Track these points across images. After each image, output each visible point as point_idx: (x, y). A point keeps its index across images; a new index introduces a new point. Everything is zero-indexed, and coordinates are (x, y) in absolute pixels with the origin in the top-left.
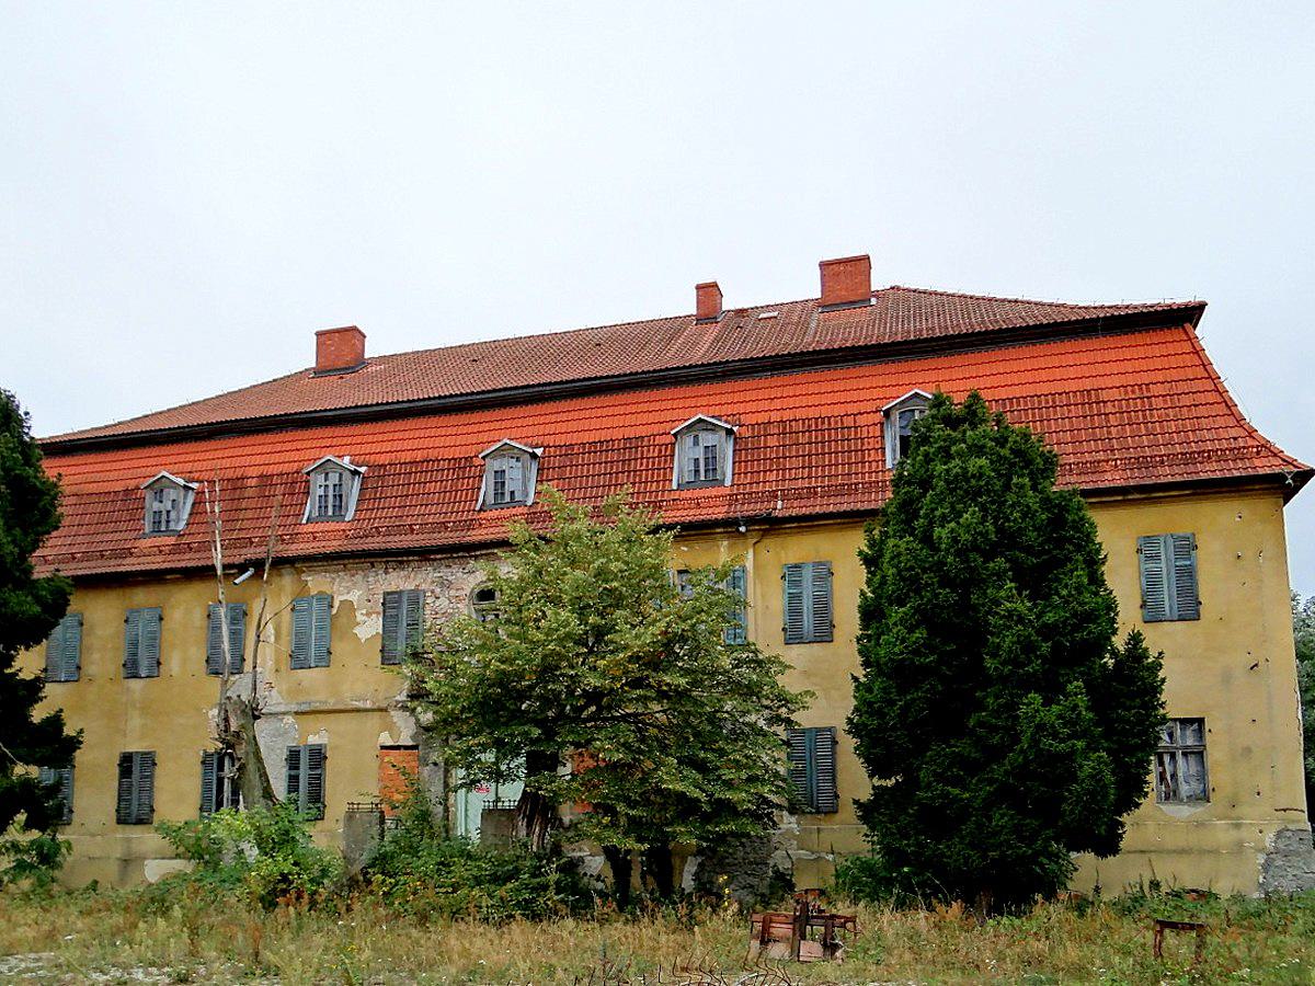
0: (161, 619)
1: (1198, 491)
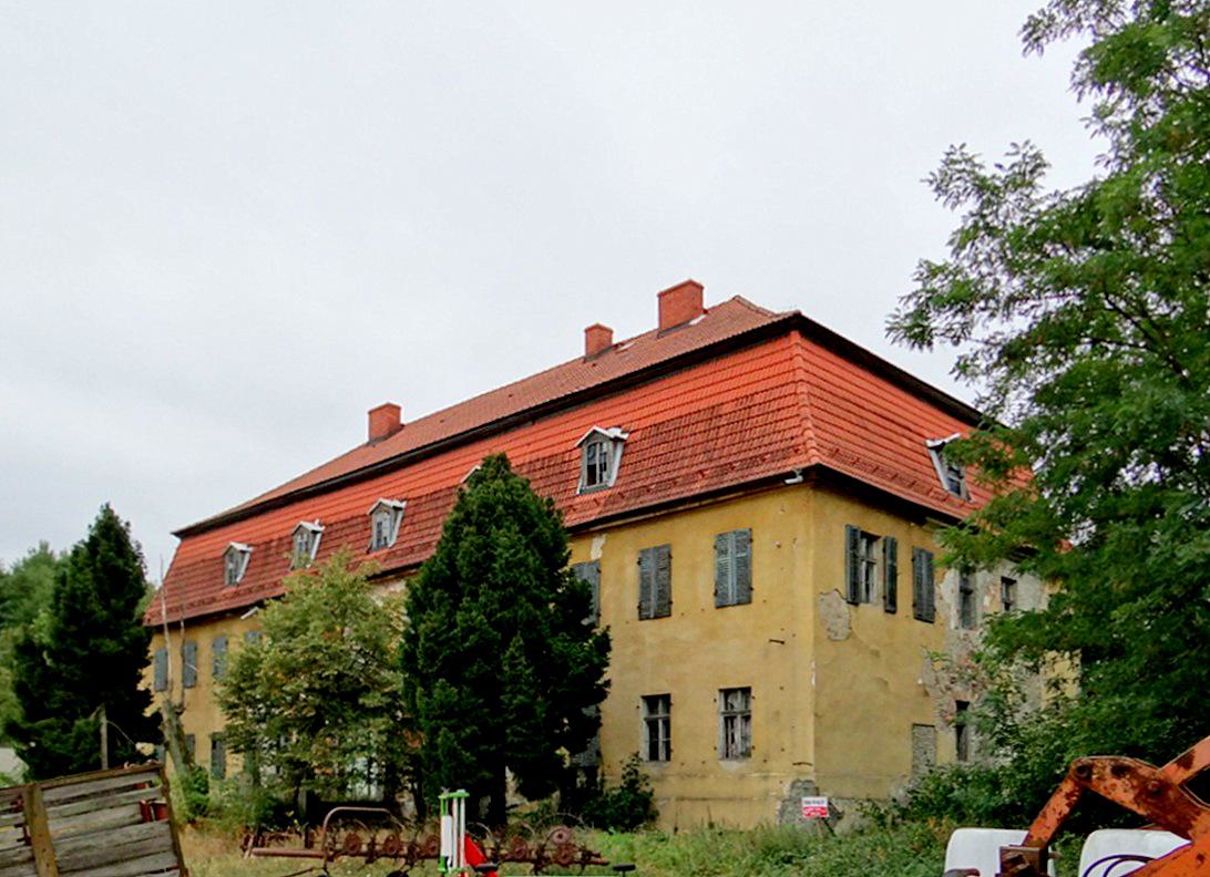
0: (196, 649)
1: (658, 514)
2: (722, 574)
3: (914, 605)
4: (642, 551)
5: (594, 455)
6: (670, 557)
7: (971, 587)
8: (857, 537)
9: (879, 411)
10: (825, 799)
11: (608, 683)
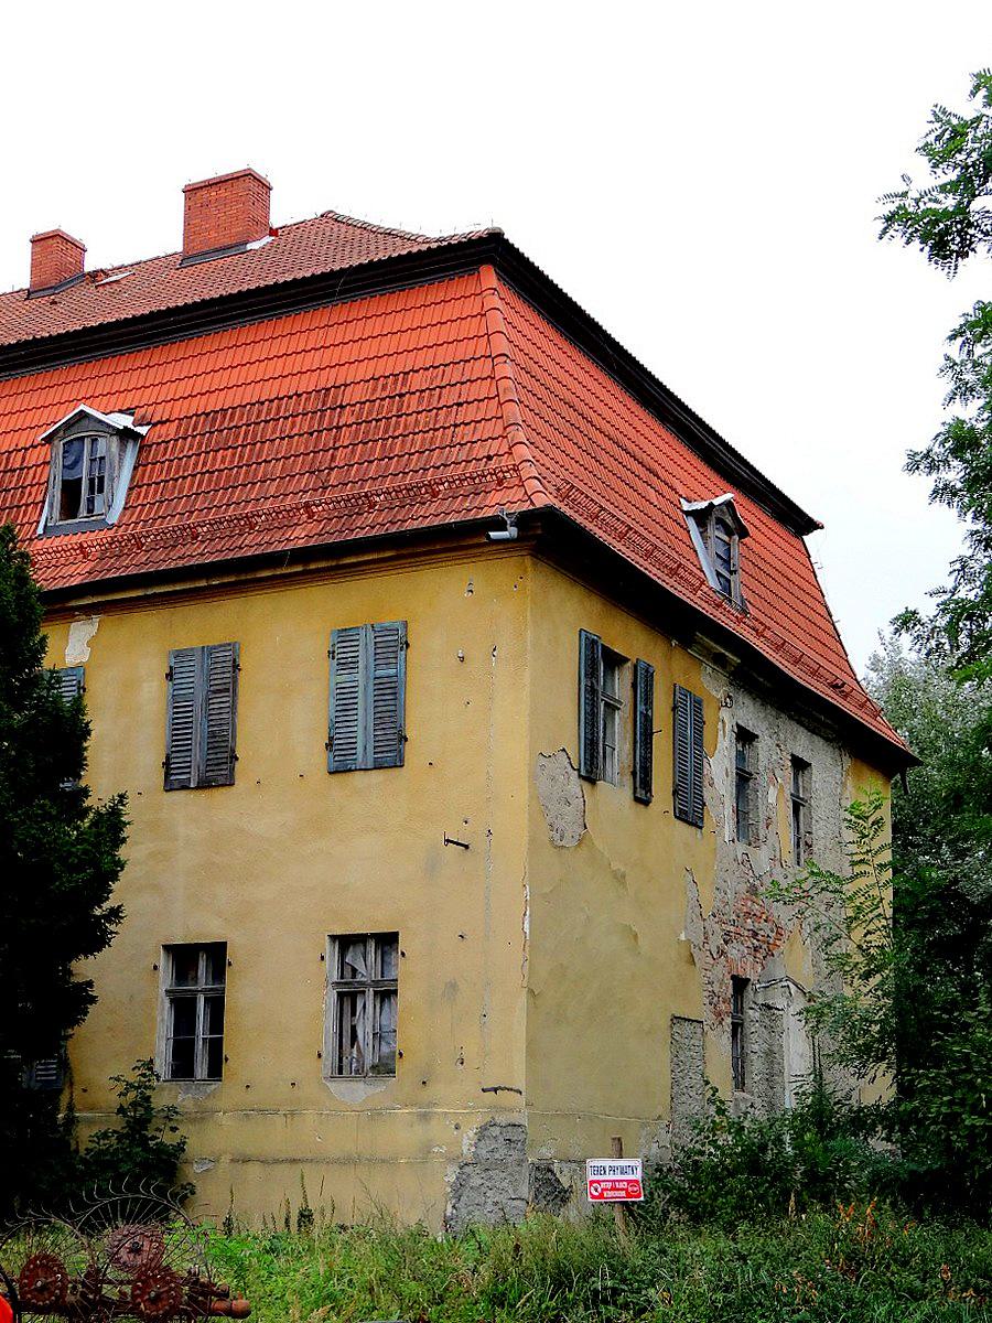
1: (404, 552)
2: (344, 703)
3: (675, 793)
4: (178, 654)
5: (77, 461)
6: (236, 667)
7: (750, 769)
8: (600, 660)
9: (612, 431)
10: (637, 1163)
11: (115, 914)
